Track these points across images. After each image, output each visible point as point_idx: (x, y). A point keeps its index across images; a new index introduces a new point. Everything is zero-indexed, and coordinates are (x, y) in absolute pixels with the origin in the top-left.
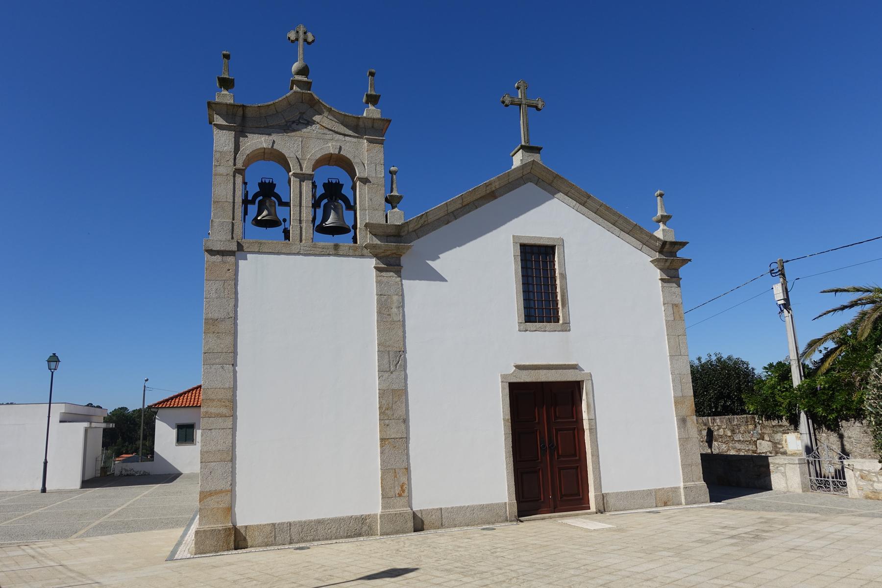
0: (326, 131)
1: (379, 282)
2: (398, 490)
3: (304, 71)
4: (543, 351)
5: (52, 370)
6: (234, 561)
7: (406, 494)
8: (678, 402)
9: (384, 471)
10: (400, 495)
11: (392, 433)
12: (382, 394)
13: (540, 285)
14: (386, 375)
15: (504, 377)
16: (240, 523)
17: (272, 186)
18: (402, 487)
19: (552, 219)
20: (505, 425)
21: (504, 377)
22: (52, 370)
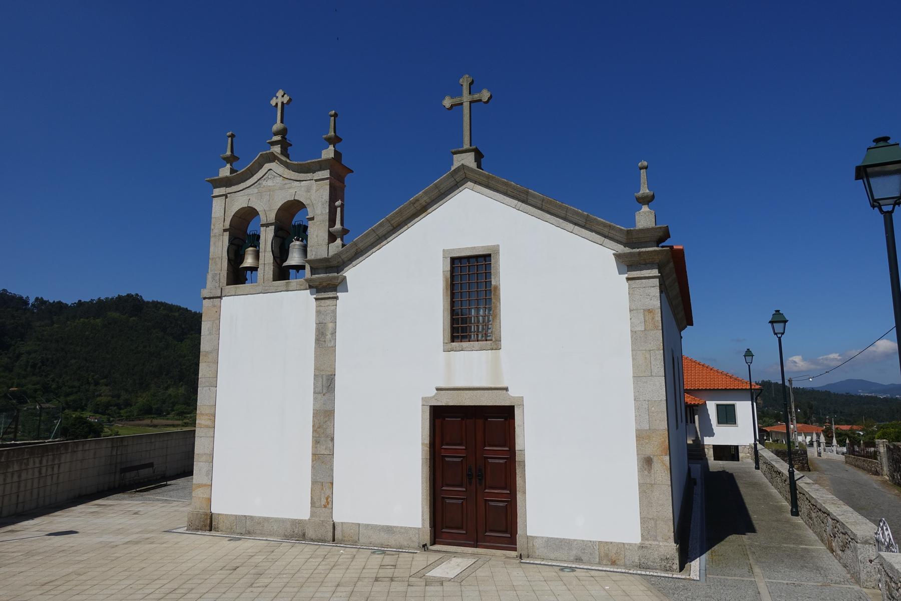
0: (287, 181)
1: (318, 313)
2: (324, 501)
3: (283, 132)
4: (470, 373)
5: (779, 335)
6: (204, 539)
7: (330, 506)
8: (641, 436)
9: (314, 482)
10: (325, 507)
11: (322, 450)
12: (316, 414)
13: (470, 295)
14: (320, 396)
15: (424, 399)
16: (213, 511)
17: (858, 169)
18: (327, 499)
19: (472, 217)
20: (423, 450)
21: (424, 399)
22: (779, 335)
